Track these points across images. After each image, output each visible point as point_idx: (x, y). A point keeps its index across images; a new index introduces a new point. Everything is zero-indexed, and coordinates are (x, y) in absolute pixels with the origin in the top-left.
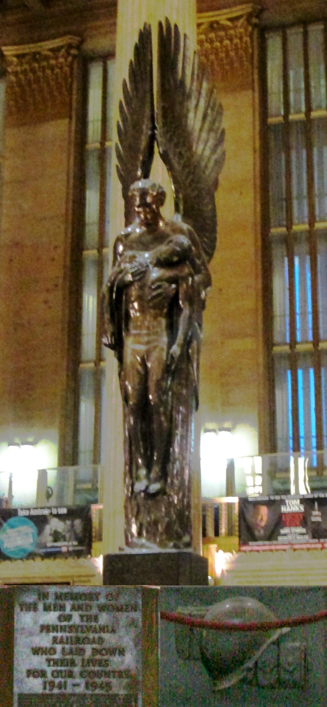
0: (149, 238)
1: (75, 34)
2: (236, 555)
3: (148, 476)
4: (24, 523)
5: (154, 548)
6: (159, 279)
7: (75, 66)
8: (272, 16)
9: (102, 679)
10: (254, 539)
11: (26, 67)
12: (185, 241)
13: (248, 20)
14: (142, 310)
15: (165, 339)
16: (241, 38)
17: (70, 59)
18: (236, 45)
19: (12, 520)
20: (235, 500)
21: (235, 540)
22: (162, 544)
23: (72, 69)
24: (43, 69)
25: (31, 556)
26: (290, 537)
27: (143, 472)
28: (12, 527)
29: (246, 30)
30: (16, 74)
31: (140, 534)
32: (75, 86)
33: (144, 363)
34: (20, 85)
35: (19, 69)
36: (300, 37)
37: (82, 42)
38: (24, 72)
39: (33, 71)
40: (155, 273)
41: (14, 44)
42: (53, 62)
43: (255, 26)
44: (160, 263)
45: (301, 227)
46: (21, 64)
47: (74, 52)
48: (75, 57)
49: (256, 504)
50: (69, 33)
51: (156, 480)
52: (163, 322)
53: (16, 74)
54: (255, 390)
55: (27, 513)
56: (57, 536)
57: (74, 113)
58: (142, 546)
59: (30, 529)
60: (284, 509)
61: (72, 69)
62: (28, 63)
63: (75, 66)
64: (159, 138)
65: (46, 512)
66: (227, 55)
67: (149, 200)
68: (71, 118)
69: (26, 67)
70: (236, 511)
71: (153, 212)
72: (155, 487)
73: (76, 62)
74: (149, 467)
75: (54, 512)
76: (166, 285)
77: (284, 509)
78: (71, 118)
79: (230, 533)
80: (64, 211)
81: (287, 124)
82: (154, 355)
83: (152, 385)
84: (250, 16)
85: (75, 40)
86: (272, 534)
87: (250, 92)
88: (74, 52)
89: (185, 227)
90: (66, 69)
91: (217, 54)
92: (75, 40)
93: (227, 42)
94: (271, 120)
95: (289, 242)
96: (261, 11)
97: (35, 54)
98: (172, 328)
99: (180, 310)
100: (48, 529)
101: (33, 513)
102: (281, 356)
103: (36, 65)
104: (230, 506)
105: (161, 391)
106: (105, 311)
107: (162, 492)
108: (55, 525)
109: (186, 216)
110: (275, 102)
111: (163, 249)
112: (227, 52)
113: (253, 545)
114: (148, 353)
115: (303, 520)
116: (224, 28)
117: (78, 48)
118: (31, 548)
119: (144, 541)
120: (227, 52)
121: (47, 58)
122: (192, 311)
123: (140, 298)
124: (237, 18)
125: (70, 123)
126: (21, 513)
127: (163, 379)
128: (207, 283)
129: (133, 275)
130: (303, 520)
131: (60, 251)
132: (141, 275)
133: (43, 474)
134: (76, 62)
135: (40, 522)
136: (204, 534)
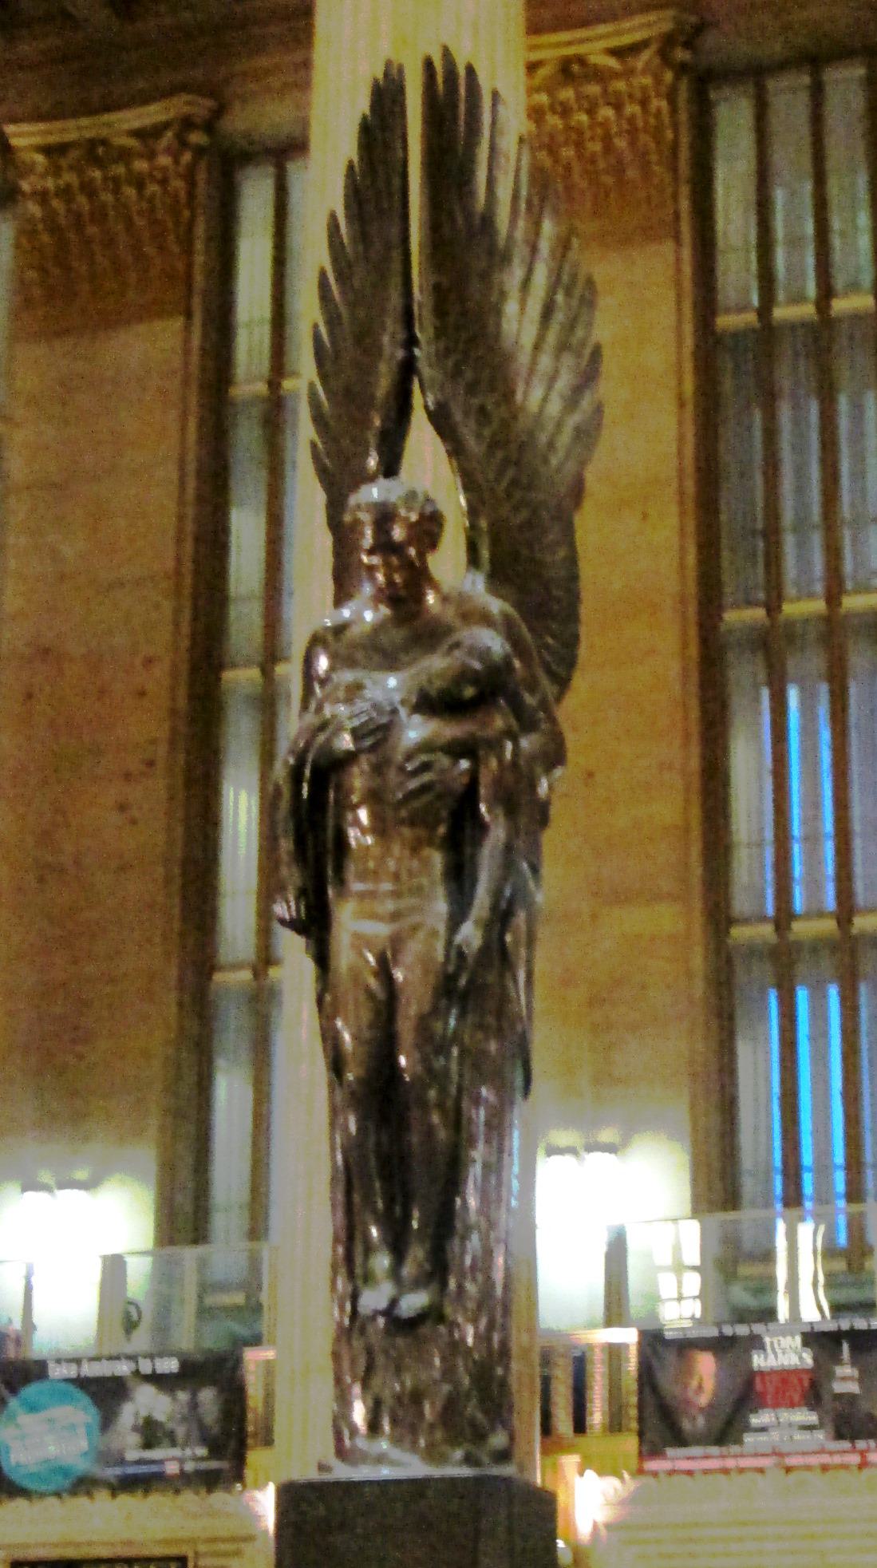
0: (398, 635)
2: (631, 1484)
3: (395, 1273)
4: (63, 1398)
5: (411, 1466)
7: (201, 176)
10: (680, 1439)
11: (70, 178)
12: (494, 643)
13: (664, 54)
14: (380, 828)
15: (441, 906)
16: (644, 103)
17: (187, 157)
19: (31, 1391)
20: (628, 1336)
21: (629, 1443)
22: (432, 1454)
23: (192, 183)
24: (116, 184)
25: (83, 1485)
26: (774, 1436)
27: (382, 1261)
28: (33, 1408)
29: (658, 80)
30: (43, 197)
31: (374, 1427)
32: (200, 230)
33: (384, 970)
34: (54, 228)
35: (50, 183)
36: (803, 101)
37: (219, 112)
38: (65, 193)
39: (89, 189)
40: (415, 731)
41: (39, 117)
42: (141, 165)
43: (682, 69)
44: (429, 704)
46: (56, 171)
47: (197, 138)
48: (199, 151)
49: (685, 1346)
50: (184, 88)
51: (417, 1284)
52: (437, 859)
53: (43, 197)
54: (682, 1043)
55: (72, 1371)
56: (151, 1433)
57: (197, 303)
58: (381, 1459)
59: (82, 1413)
61: (192, 183)
63: (201, 176)
64: (425, 369)
65: (123, 1369)
66: (608, 147)
67: (398, 533)
68: (189, 315)
69: (70, 178)
72: (414, 1302)
73: (203, 165)
74: (398, 1247)
75: (146, 1367)
76: (444, 761)
77: (758, 1361)
78: (189, 315)
79: (615, 1425)
81: (767, 332)
82: (413, 949)
83: (406, 1028)
84: (668, 42)
85: (200, 107)
86: (727, 1428)
88: (197, 138)
89: (496, 606)
90: (178, 184)
92: (200, 107)
93: (607, 112)
94: (726, 322)
96: (699, 29)
97: (93, 143)
98: (460, 877)
99: (482, 828)
100: (129, 1414)
101: (89, 1370)
102: (752, 951)
103: (97, 174)
104: (615, 1352)
105: (431, 1044)
107: (433, 1315)
108: (148, 1402)
109: (499, 578)
110: (736, 272)
111: (437, 664)
112: (607, 140)
113: (677, 1458)
114: (397, 942)
115: (811, 1389)
117: (209, 127)
118: (83, 1465)
119: (384, 1445)
120: (607, 140)
121: (125, 155)
122: (514, 832)
123: (374, 798)
124: (635, 49)
125: (187, 328)
126: (56, 1372)
127: (436, 1012)
128: (554, 756)
129: (356, 734)
130: (811, 1389)
132: (377, 734)
134: (203, 165)
135: (106, 1394)
136: (547, 1428)
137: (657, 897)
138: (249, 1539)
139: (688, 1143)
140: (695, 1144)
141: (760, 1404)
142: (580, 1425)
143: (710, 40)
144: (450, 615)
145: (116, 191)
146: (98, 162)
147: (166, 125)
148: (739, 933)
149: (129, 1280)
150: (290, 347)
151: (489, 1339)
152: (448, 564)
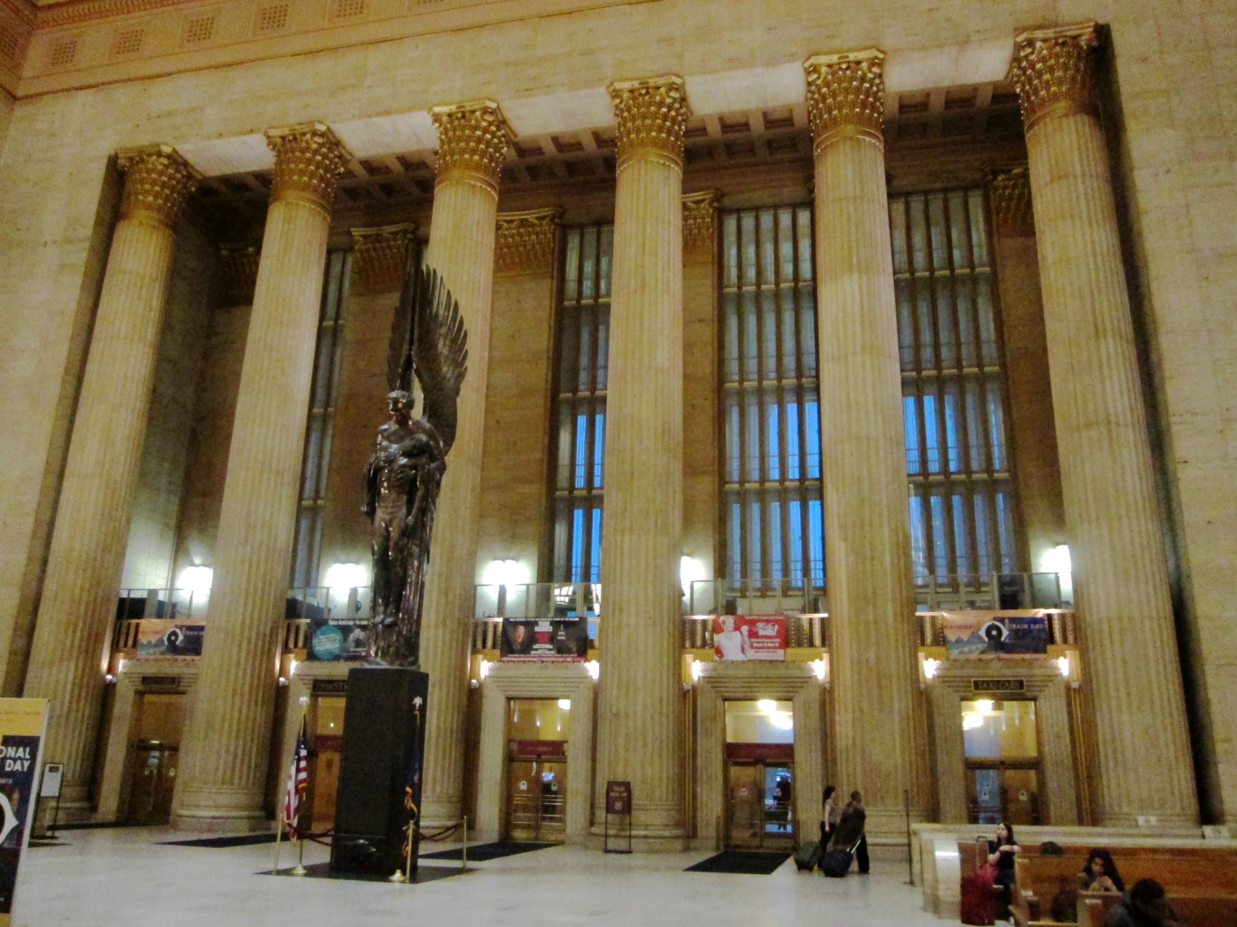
0: (402, 433)
1: (414, 222)
2: (498, 664)
3: (385, 613)
4: (332, 631)
5: (385, 665)
6: (403, 466)
8: (571, 217)
10: (512, 652)
11: (370, 246)
12: (424, 438)
13: (552, 220)
14: (389, 488)
15: (404, 511)
19: (324, 628)
20: (500, 620)
21: (498, 652)
22: (392, 663)
24: (383, 249)
25: (337, 658)
26: (540, 652)
27: (381, 609)
28: (323, 634)
30: (361, 251)
31: (376, 654)
33: (387, 529)
34: (364, 260)
36: (595, 236)
37: (417, 229)
38: (368, 251)
39: (375, 249)
40: (404, 461)
41: (364, 226)
42: (392, 243)
43: (557, 225)
44: (405, 454)
45: (584, 393)
47: (410, 236)
48: (410, 240)
49: (516, 624)
50: (404, 221)
51: (391, 615)
52: (405, 498)
53: (361, 251)
54: (534, 528)
55: (335, 623)
56: (358, 643)
58: (378, 664)
59: (337, 636)
60: (537, 629)
61: (407, 250)
62: (373, 242)
64: (414, 359)
65: (351, 623)
67: (400, 405)
69: (370, 246)
70: (500, 629)
71: (402, 415)
72: (389, 620)
74: (386, 606)
75: (358, 623)
76: (407, 470)
77: (537, 629)
79: (494, 647)
81: (579, 308)
82: (395, 523)
83: (391, 544)
84: (554, 217)
85: (411, 227)
86: (526, 648)
87: (549, 281)
88: (410, 236)
89: (428, 425)
90: (402, 250)
92: (411, 227)
93: (534, 237)
94: (566, 303)
95: (574, 407)
96: (563, 213)
97: (378, 235)
98: (410, 503)
99: (417, 489)
100: (352, 637)
101: (341, 623)
102: (562, 499)
104: (495, 626)
105: (400, 549)
107: (394, 624)
108: (358, 634)
109: (430, 419)
110: (571, 287)
111: (408, 443)
112: (533, 245)
113: (511, 657)
114: (391, 520)
115: (552, 638)
117: (413, 232)
118: (337, 652)
119: (378, 660)
120: (533, 245)
121: (387, 240)
122: (427, 489)
123: (388, 480)
124: (545, 217)
126: (331, 623)
127: (400, 539)
128: (442, 469)
129: (385, 462)
130: (552, 638)
132: (391, 461)
133: (354, 592)
135: (345, 631)
136: (474, 646)
137: (532, 482)
139: (536, 558)
140: (539, 558)
141: (536, 642)
142: (484, 646)
144: (414, 428)
148: (558, 493)
152: (417, 413)
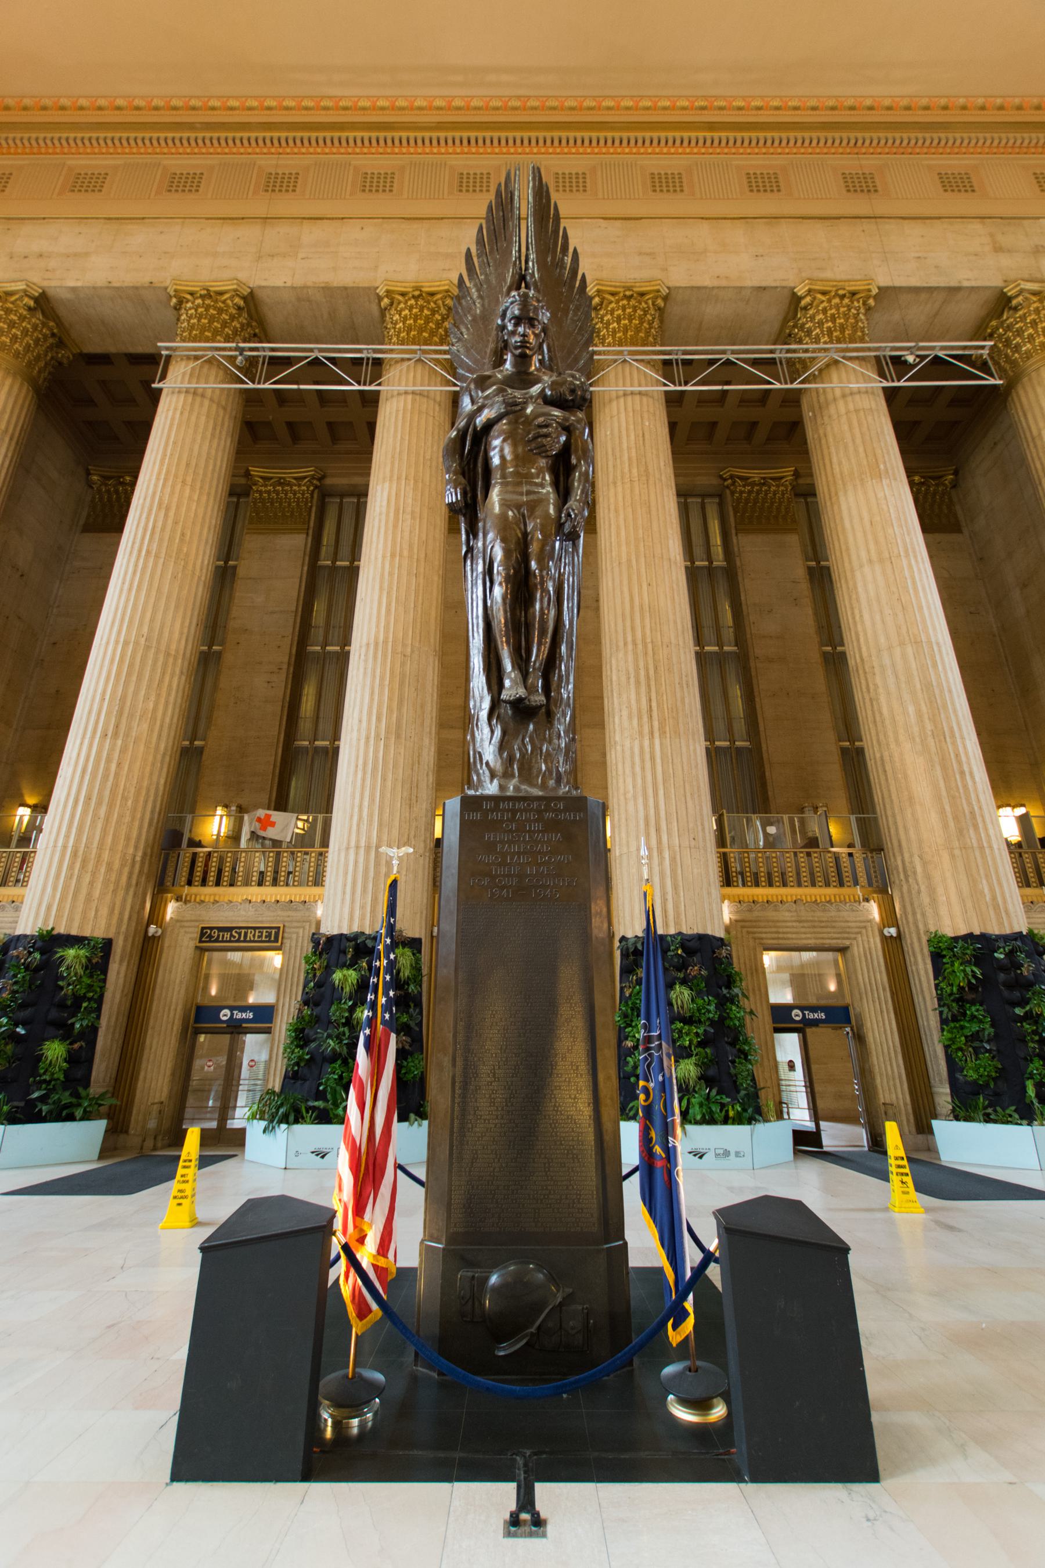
7: (315, 496)
9: (491, 339)
16: (303, 494)
17: (312, 488)
18: (298, 498)
23: (312, 497)
29: (308, 488)
32: (314, 509)
35: (263, 489)
46: (299, 485)
48: (316, 487)
57: (311, 532)
63: (315, 496)
66: (298, 505)
68: (307, 534)
73: (316, 491)
78: (307, 534)
80: (294, 609)
91: (281, 503)
93: (290, 495)
97: (280, 478)
103: (280, 488)
106: (321, 631)
116: (289, 484)
120: (298, 502)
125: (307, 539)
131: (288, 641)
134: (316, 491)
138: (870, 921)
143: (328, 481)
145: (286, 495)
146: (280, 484)
147: (305, 477)
149: (328, 1306)
150: (711, 535)
151: (588, 1323)
